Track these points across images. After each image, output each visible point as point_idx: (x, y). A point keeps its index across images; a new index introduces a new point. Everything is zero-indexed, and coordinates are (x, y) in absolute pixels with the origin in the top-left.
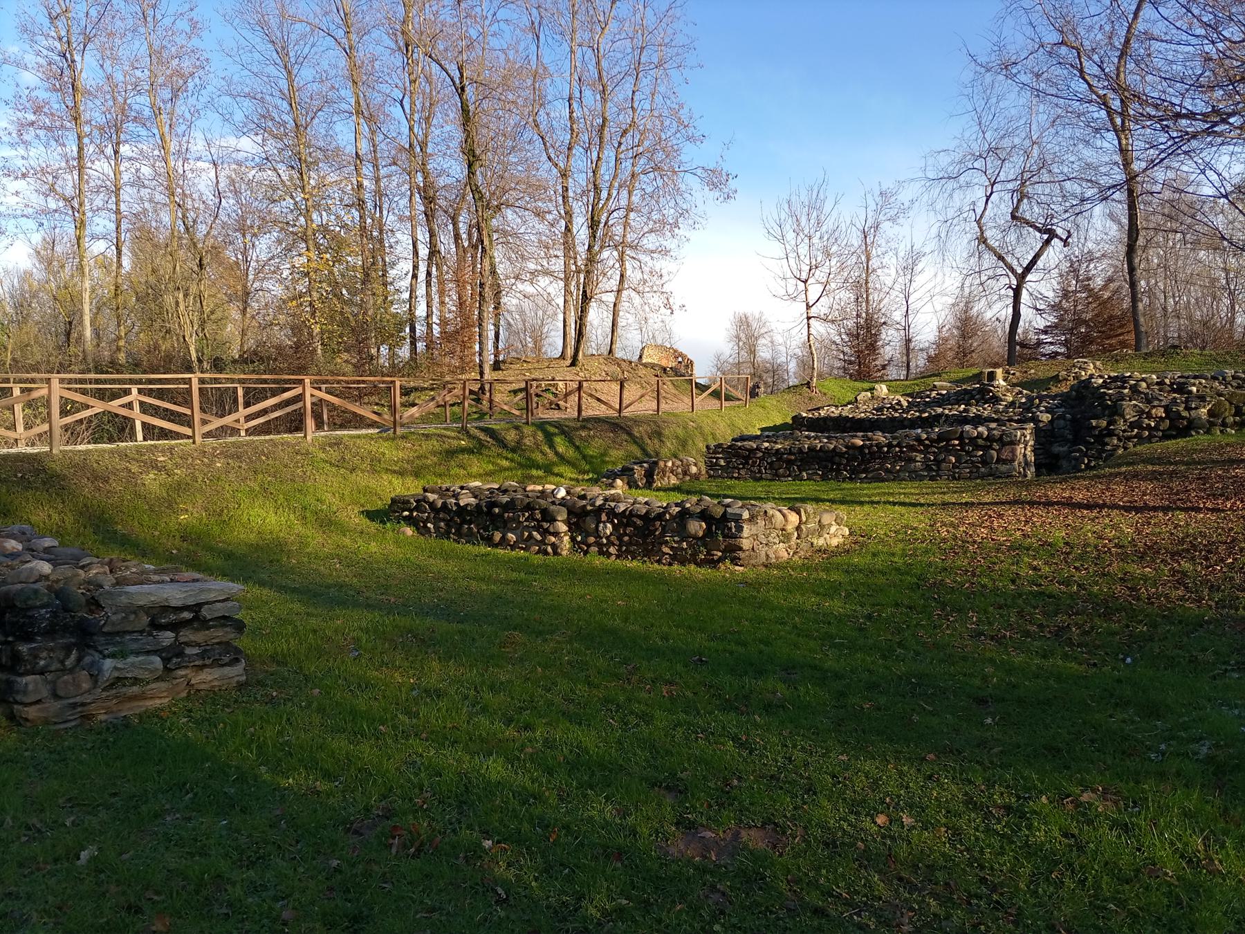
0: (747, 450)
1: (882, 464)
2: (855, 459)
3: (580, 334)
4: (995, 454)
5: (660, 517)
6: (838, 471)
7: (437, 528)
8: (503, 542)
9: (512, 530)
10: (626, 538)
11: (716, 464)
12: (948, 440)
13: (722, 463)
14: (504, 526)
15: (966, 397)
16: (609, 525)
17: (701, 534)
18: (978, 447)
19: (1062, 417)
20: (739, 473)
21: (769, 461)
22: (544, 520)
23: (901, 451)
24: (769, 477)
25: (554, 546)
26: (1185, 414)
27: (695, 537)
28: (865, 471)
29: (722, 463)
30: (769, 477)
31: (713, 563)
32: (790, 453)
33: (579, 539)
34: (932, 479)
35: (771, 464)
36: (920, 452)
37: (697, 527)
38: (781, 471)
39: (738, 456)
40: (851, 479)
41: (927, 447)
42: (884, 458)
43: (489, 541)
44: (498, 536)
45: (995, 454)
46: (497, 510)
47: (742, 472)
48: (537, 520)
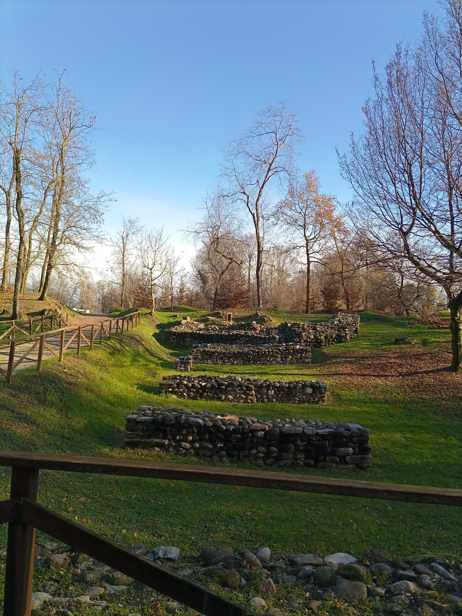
0: (211, 352)
1: (266, 358)
2: (256, 356)
3: (46, 284)
4: (304, 355)
5: (295, 387)
6: (249, 361)
7: (188, 395)
8: (227, 399)
9: (230, 394)
10: (280, 396)
11: (197, 358)
12: (289, 350)
13: (200, 357)
14: (226, 392)
15: (243, 327)
16: (273, 391)
17: (311, 392)
18: (299, 353)
19: (282, 337)
20: (207, 362)
21: (221, 356)
22: (247, 390)
23: (273, 354)
24: (221, 363)
25: (250, 399)
26: (319, 338)
27: (309, 394)
28: (259, 361)
29: (200, 357)
30: (221, 363)
31: (317, 403)
32: (230, 354)
33: (259, 396)
34: (284, 364)
35: (222, 358)
36: (280, 354)
37: (309, 390)
38: (226, 361)
39: (207, 354)
40: (254, 364)
41: (282, 352)
42: (267, 356)
43: (219, 399)
44: (224, 397)
45: (304, 355)
46: (224, 387)
47: (209, 361)
48: (244, 390)
